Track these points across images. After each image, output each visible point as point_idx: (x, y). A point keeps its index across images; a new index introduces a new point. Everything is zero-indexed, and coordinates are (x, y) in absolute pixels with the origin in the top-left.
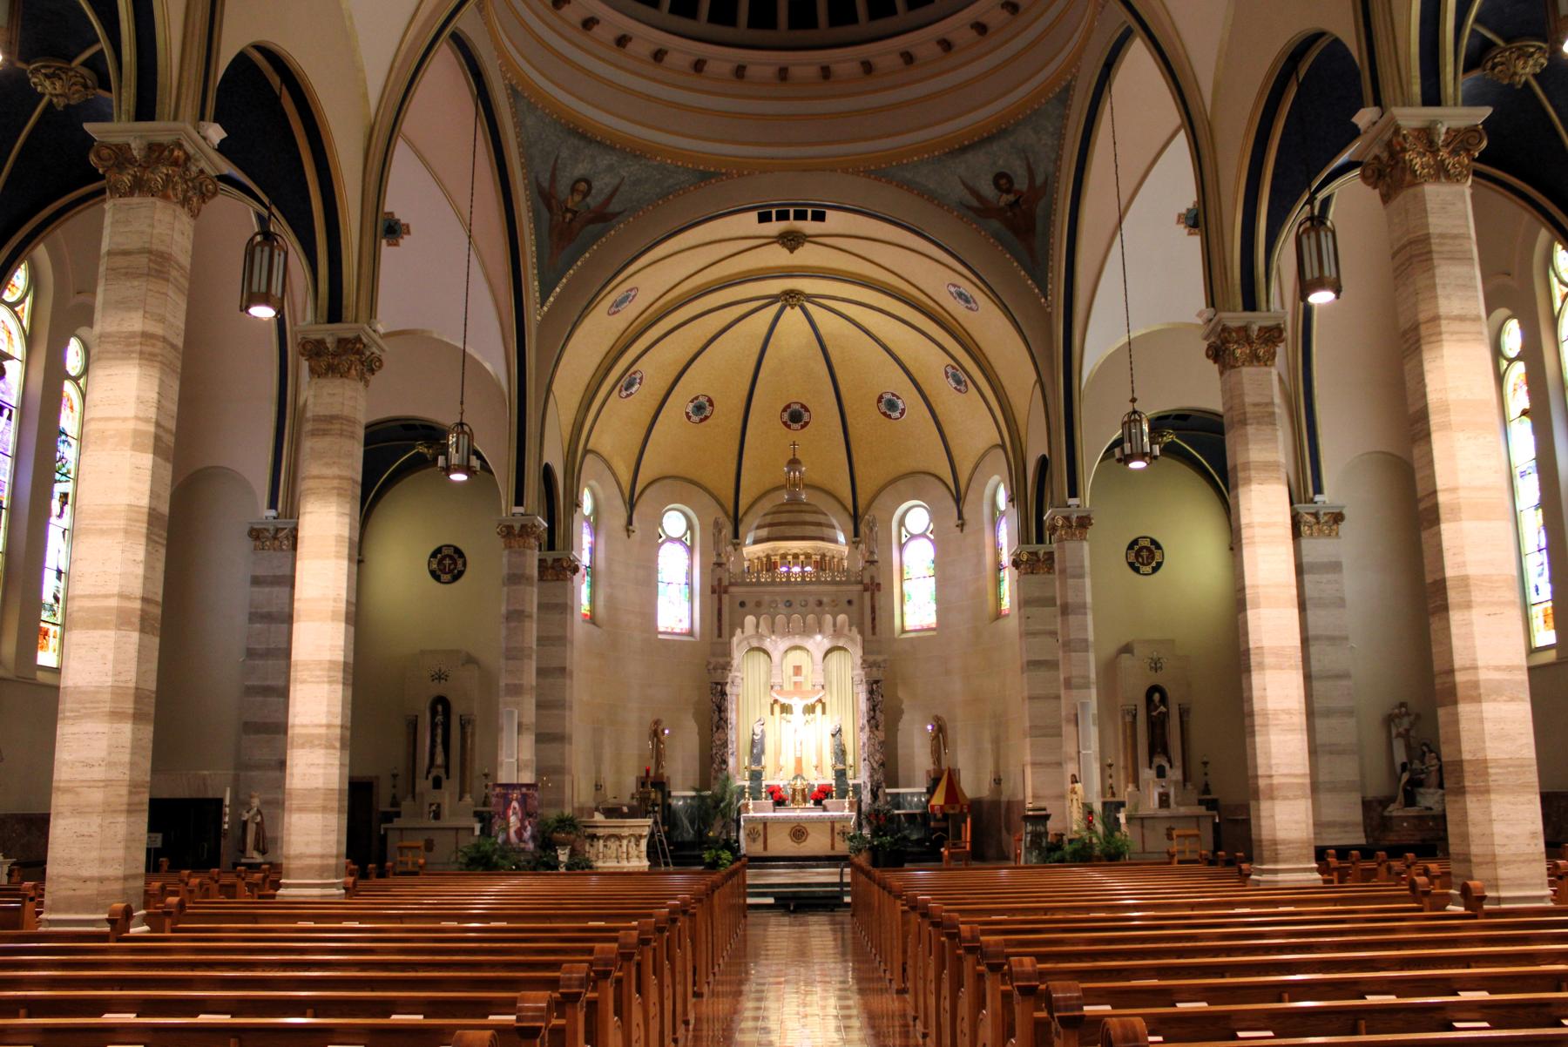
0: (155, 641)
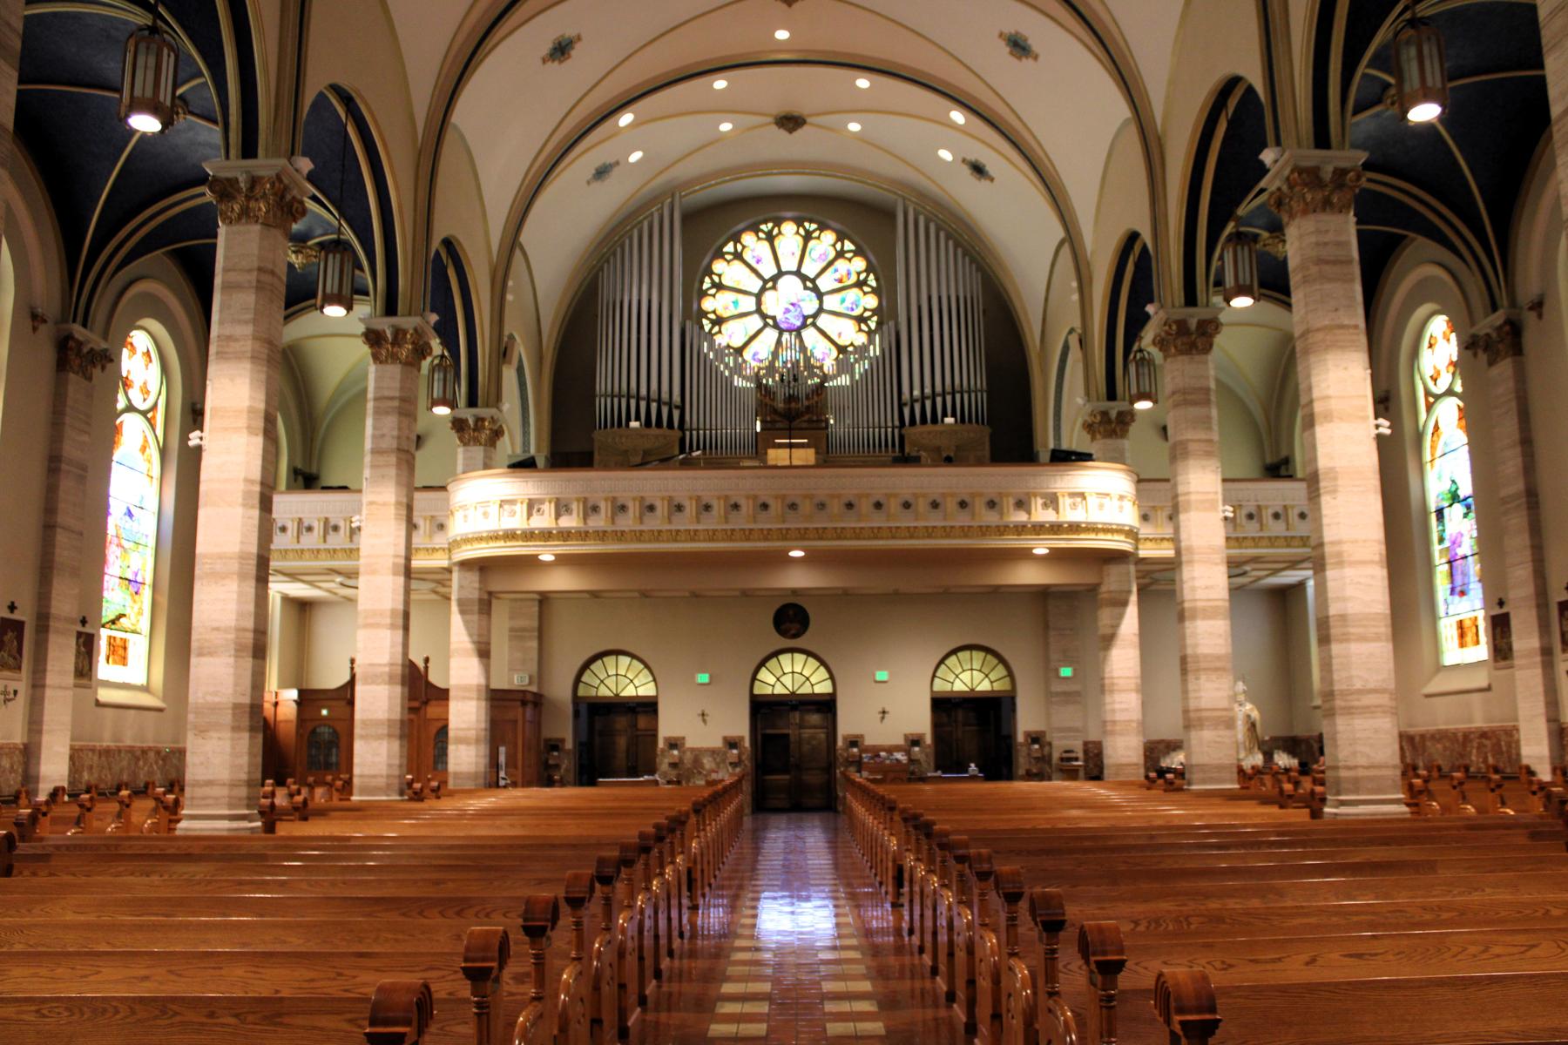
0: (406, 690)
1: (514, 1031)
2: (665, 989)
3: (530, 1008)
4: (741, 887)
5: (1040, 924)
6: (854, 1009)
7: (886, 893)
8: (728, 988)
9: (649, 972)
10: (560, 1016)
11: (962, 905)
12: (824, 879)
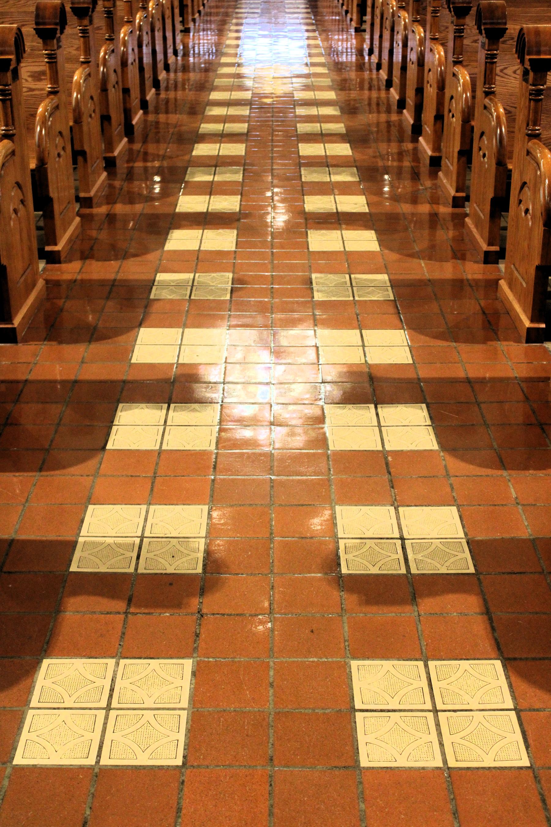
1: (35, 119)
2: (163, 95)
3: (47, 101)
4: (227, 15)
5: (483, 32)
6: (320, 113)
7: (351, 20)
8: (215, 96)
9: (149, 82)
10: (74, 110)
11: (416, 24)
12: (298, 8)
